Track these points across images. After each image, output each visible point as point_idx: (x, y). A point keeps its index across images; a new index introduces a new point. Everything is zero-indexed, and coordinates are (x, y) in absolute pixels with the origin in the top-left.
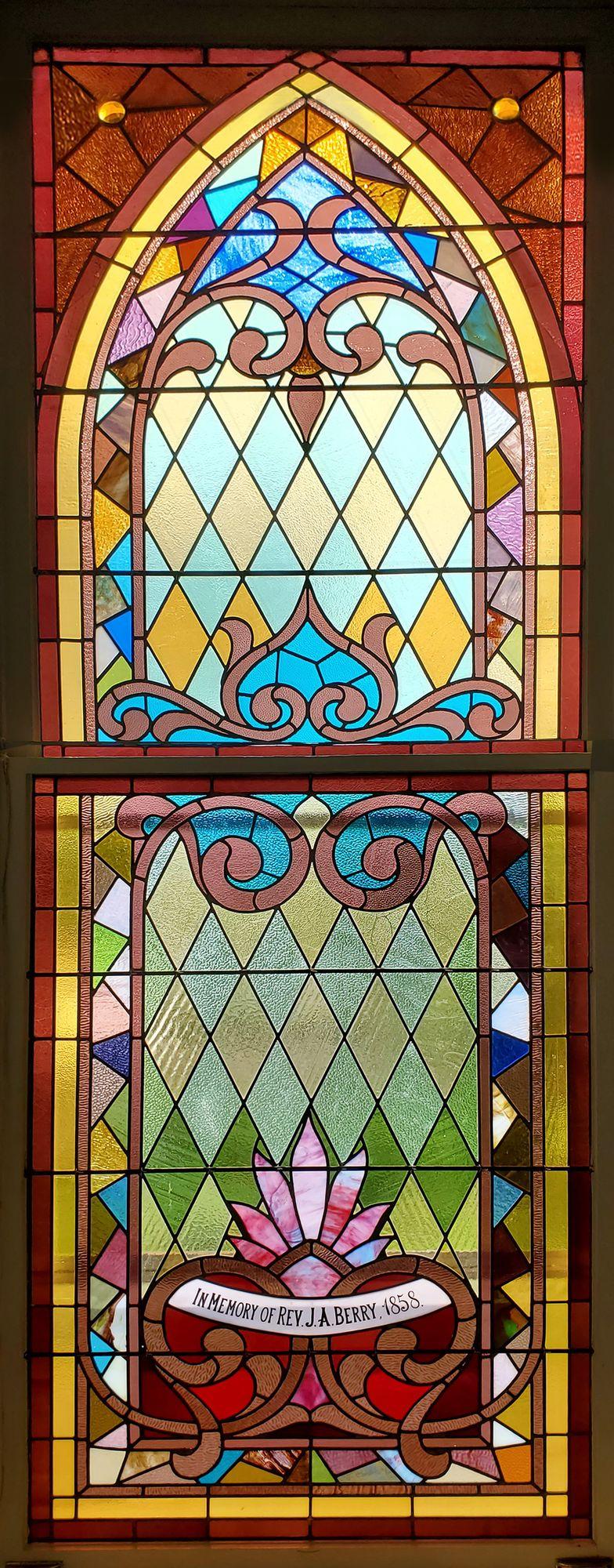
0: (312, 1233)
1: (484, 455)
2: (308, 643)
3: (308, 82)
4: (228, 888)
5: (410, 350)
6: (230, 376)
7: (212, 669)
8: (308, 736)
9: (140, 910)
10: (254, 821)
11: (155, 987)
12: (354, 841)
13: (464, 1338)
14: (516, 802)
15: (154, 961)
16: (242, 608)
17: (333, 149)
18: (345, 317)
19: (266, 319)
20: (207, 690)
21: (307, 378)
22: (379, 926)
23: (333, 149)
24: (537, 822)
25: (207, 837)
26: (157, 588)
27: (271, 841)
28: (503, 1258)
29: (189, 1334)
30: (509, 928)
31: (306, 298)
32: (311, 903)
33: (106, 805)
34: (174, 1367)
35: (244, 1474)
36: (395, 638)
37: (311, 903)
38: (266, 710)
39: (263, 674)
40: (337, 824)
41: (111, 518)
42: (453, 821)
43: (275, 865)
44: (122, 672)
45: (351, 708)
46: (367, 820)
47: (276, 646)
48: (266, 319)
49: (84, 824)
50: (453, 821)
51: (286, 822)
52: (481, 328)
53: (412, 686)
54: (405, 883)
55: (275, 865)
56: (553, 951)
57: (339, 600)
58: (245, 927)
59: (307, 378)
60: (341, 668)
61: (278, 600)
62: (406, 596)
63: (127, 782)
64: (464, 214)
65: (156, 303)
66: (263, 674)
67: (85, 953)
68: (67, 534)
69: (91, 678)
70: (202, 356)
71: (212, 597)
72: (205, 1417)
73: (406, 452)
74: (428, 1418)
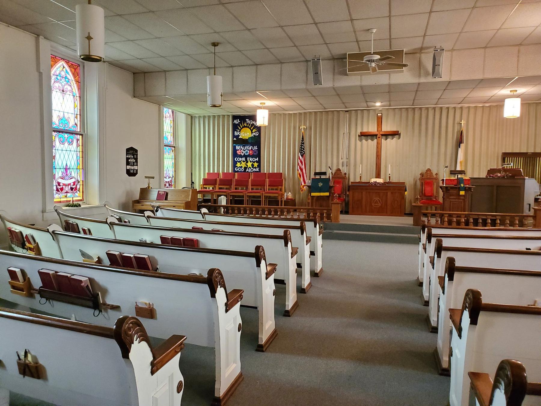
4: (62, 142)
6: (58, 91)
22: (70, 146)
30: (78, 145)
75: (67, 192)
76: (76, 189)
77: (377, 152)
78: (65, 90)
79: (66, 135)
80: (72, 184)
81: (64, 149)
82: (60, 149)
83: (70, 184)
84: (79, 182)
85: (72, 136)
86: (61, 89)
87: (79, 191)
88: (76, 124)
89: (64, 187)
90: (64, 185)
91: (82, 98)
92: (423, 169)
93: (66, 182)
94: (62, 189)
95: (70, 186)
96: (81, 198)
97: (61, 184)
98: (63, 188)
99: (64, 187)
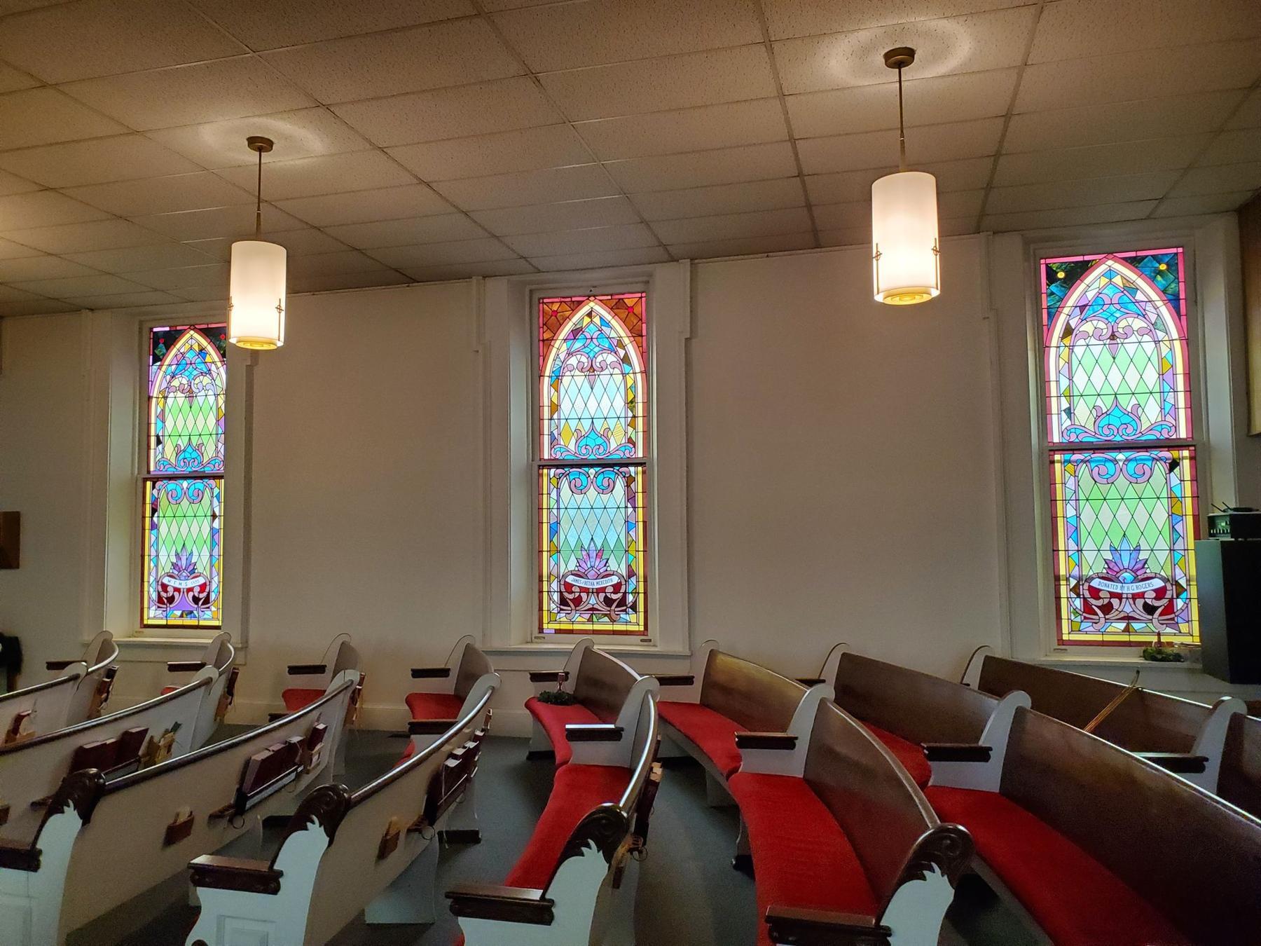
0: (1126, 565)
1: (1161, 359)
2: (190, 450)
3: (1110, 262)
4: (577, 489)
5: (1141, 332)
6: (577, 373)
7: (573, 441)
8: (1118, 438)
9: (558, 495)
10: (1108, 460)
11: (562, 511)
12: (1132, 465)
13: (1169, 595)
14: (632, 469)
15: (562, 506)
16: (580, 427)
17: (1118, 280)
18: (1123, 324)
19: (1101, 325)
20: (572, 447)
21: (591, 371)
22: (605, 497)
23: (1118, 280)
24: (636, 473)
25: (1093, 465)
26: (563, 422)
27: (1110, 465)
28: (631, 573)
29: (569, 587)
30: (631, 498)
31: (592, 355)
32: (592, 492)
33: (553, 471)
34: (566, 595)
35: (580, 619)
36: (1140, 410)
37: (592, 492)
38: (584, 451)
39: (1104, 422)
40: (1128, 460)
41: (160, 424)
42: (1159, 459)
43: (1111, 472)
44: (1068, 423)
45: (1130, 430)
46: (1135, 459)
47: (1107, 414)
48: (584, 359)
49: (548, 475)
50: (1159, 459)
51: (1115, 461)
52: (626, 360)
53: (613, 445)
54: (610, 488)
55: (1112, 471)
56: (640, 503)
57: (599, 425)
58: (579, 497)
59: (591, 371)
60: (1126, 419)
61: (586, 424)
62: (205, 439)
63: (557, 467)
64: (623, 334)
65: (562, 356)
66: (1104, 422)
67: (549, 503)
68: (1053, 385)
69: (1060, 424)
70: (1086, 336)
71: (573, 424)
72: (1101, 615)
73: (1140, 359)
74: (1161, 615)
75: (593, 609)
76: (622, 602)
77: (247, 620)
78: (597, 365)
79: (185, 484)
80: (197, 590)
81: (585, 504)
82: (573, 504)
83: (603, 590)
84: (1180, 590)
85: (199, 484)
86: (1106, 333)
87: (634, 607)
88: (630, 440)
89: (584, 595)
90: (583, 590)
91: (1193, 342)
92: (40, 871)
93: (184, 585)
94: (578, 601)
95: (602, 596)
96: (1065, 637)
97: (170, 590)
98: (580, 598)
99: (584, 595)
